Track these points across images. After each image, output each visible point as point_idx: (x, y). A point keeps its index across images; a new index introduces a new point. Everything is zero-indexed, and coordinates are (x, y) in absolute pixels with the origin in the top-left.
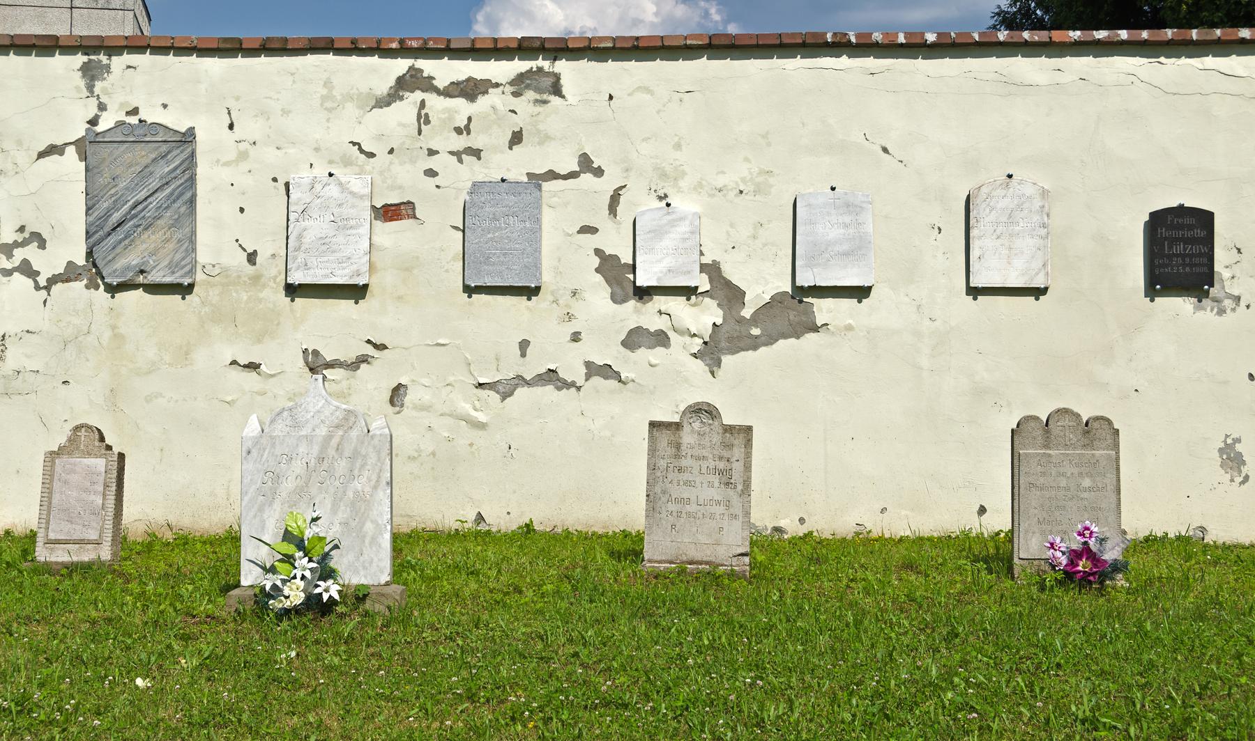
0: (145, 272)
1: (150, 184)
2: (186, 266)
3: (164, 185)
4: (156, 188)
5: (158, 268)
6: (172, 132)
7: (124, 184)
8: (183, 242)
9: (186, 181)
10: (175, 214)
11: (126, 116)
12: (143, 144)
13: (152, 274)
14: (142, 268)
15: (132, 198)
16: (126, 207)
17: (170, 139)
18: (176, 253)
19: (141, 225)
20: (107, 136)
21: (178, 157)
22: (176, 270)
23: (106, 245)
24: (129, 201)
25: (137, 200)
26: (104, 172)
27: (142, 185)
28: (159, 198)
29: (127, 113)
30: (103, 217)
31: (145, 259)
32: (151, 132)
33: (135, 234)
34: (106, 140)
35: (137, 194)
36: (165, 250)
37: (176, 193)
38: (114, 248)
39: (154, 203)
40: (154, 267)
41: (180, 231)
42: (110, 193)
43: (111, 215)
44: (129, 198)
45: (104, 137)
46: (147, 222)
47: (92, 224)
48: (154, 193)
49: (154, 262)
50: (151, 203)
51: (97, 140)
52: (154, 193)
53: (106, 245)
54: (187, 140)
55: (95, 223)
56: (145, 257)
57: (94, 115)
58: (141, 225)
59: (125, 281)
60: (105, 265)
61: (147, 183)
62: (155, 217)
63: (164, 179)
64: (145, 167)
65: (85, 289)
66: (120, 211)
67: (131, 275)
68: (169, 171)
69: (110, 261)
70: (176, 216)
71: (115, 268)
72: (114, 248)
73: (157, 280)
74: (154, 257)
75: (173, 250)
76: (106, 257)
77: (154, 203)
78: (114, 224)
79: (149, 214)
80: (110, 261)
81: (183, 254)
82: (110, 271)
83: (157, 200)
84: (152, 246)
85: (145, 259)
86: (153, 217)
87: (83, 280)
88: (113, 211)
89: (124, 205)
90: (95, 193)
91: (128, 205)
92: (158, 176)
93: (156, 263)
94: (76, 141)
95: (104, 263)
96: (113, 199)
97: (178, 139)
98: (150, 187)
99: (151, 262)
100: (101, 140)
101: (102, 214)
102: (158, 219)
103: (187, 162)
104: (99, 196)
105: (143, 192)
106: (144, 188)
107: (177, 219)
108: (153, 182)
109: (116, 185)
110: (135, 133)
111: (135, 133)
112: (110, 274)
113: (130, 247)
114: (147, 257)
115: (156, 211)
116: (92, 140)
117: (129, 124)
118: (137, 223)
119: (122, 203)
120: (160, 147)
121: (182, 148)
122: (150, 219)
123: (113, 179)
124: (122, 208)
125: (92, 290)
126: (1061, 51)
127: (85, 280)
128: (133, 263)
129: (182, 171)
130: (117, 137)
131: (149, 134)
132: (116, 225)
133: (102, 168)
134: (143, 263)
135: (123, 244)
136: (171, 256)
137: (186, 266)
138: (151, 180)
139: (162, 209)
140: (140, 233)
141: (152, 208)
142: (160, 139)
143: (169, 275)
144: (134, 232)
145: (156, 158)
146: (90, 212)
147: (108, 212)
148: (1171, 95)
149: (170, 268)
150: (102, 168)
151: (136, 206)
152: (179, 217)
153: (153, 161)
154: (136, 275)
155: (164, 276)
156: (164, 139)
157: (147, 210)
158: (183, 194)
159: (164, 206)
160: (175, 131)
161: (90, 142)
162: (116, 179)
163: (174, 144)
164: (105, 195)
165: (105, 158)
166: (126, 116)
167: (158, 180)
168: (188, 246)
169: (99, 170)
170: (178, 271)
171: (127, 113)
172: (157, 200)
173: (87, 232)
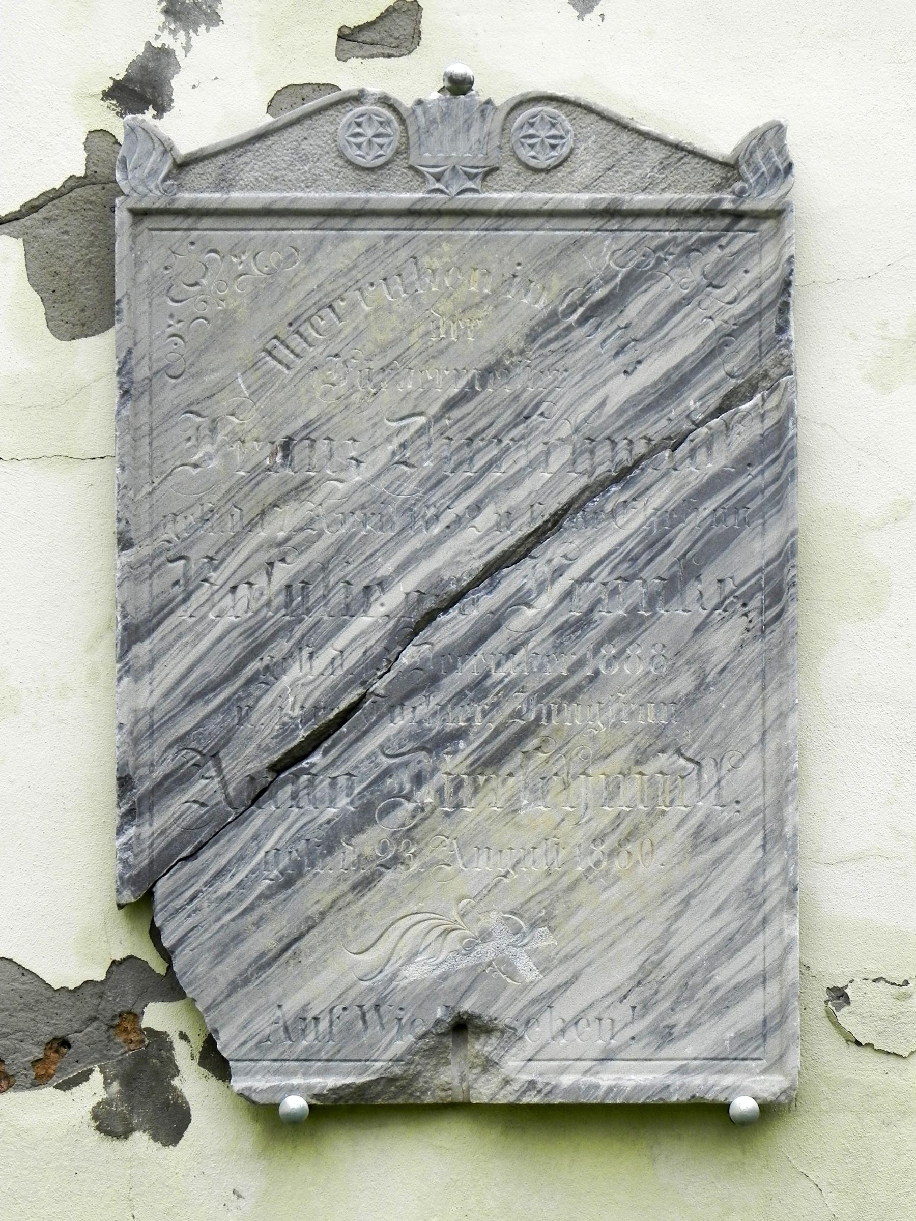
0: (486, 1029)
1: (515, 480)
2: (740, 991)
3: (601, 487)
4: (553, 506)
5: (567, 1007)
6: (655, 154)
7: (356, 477)
8: (725, 843)
9: (745, 462)
10: (673, 672)
11: (341, 56)
12: (471, 232)
13: (530, 1043)
14: (467, 1006)
15: (403, 568)
16: (362, 622)
17: (640, 200)
18: (678, 916)
19: (459, 735)
20: (248, 176)
21: (693, 315)
22: (682, 1017)
23: (240, 858)
24: (382, 584)
25: (436, 582)
26: (226, 401)
27: (468, 486)
28: (577, 570)
29: (346, 36)
30: (227, 678)
31: (487, 951)
32: (525, 154)
33: (426, 795)
34: (238, 197)
35: (431, 547)
36: (614, 894)
37: (681, 540)
38: (288, 882)
39: (545, 602)
40: (547, 1000)
41: (709, 774)
42: (262, 534)
43: (273, 672)
44: (387, 568)
45: (224, 183)
46: (499, 717)
47: (152, 731)
48: (539, 535)
49: (545, 969)
50: (522, 600)
51: (185, 198)
52: (539, 535)
53: (240, 858)
54: (747, 206)
55: (171, 719)
56: (485, 936)
57: (141, 50)
58: (459, 735)
59: (362, 1089)
60: (233, 988)
61: (495, 475)
62: (548, 688)
63: (604, 451)
64: (487, 373)
65: (94, 1138)
66: (330, 652)
67: (400, 1046)
68: (632, 401)
69: (264, 963)
70: (684, 683)
71: (292, 1006)
72: (288, 882)
73: (566, 1080)
74: (544, 940)
75: (666, 894)
76: (238, 938)
77: (545, 602)
78: (286, 730)
79: (509, 670)
80: (264, 963)
81: (730, 920)
82: (263, 1024)
83: (564, 583)
84: (534, 868)
85: (487, 951)
86: (534, 684)
87: (84, 1077)
88: (283, 646)
89: (349, 611)
90: (168, 533)
91: (377, 611)
92: (565, 430)
93: (558, 976)
94: (31, 208)
95: (228, 970)
96: (282, 573)
97: (697, 198)
98: (518, 495)
99: (526, 968)
100: (211, 198)
101: (213, 668)
102: (571, 696)
103: (748, 343)
104: (196, 555)
105: (470, 533)
106: (477, 508)
107: (691, 700)
108: (532, 466)
109: (302, 488)
110: (424, 157)
111: (424, 157)
112: (263, 1043)
113: (389, 875)
114: (502, 939)
115: (559, 649)
116: (154, 198)
117: (386, 101)
118: (435, 726)
119: (338, 598)
120: (578, 244)
121: (714, 254)
122: (517, 702)
123: (287, 446)
124: (340, 627)
125: (141, 1140)
126: (744, 1152)
127: (97, 1077)
128: (414, 973)
129: (714, 401)
130: (311, 183)
131: (509, 168)
132: (303, 734)
133: (211, 379)
134: (476, 976)
135: (347, 854)
136: (651, 928)
137: (740, 991)
138: (520, 458)
139: (593, 635)
140: (458, 786)
141: (532, 630)
142: (582, 199)
143: (635, 1050)
144: (419, 780)
145: (552, 319)
146: (142, 650)
147: (254, 653)
148: (88, 461)
149: (647, 1006)
150: (211, 379)
151: (430, 617)
152: (702, 686)
153: (532, 337)
154: (431, 1052)
155: (606, 1058)
156: (603, 197)
157: (499, 641)
158: (725, 541)
159: (607, 616)
160: (677, 147)
161: (139, 214)
162: (300, 451)
163: (666, 230)
164: (232, 545)
165: (229, 314)
166: (341, 56)
167: (567, 451)
168: (761, 867)
169: (191, 390)
170: (691, 1026)
171: (346, 36)
172: (564, 583)
173: (125, 782)
